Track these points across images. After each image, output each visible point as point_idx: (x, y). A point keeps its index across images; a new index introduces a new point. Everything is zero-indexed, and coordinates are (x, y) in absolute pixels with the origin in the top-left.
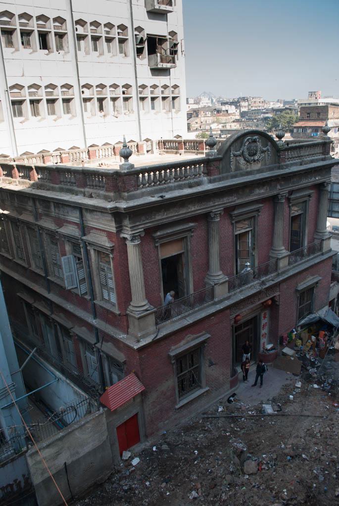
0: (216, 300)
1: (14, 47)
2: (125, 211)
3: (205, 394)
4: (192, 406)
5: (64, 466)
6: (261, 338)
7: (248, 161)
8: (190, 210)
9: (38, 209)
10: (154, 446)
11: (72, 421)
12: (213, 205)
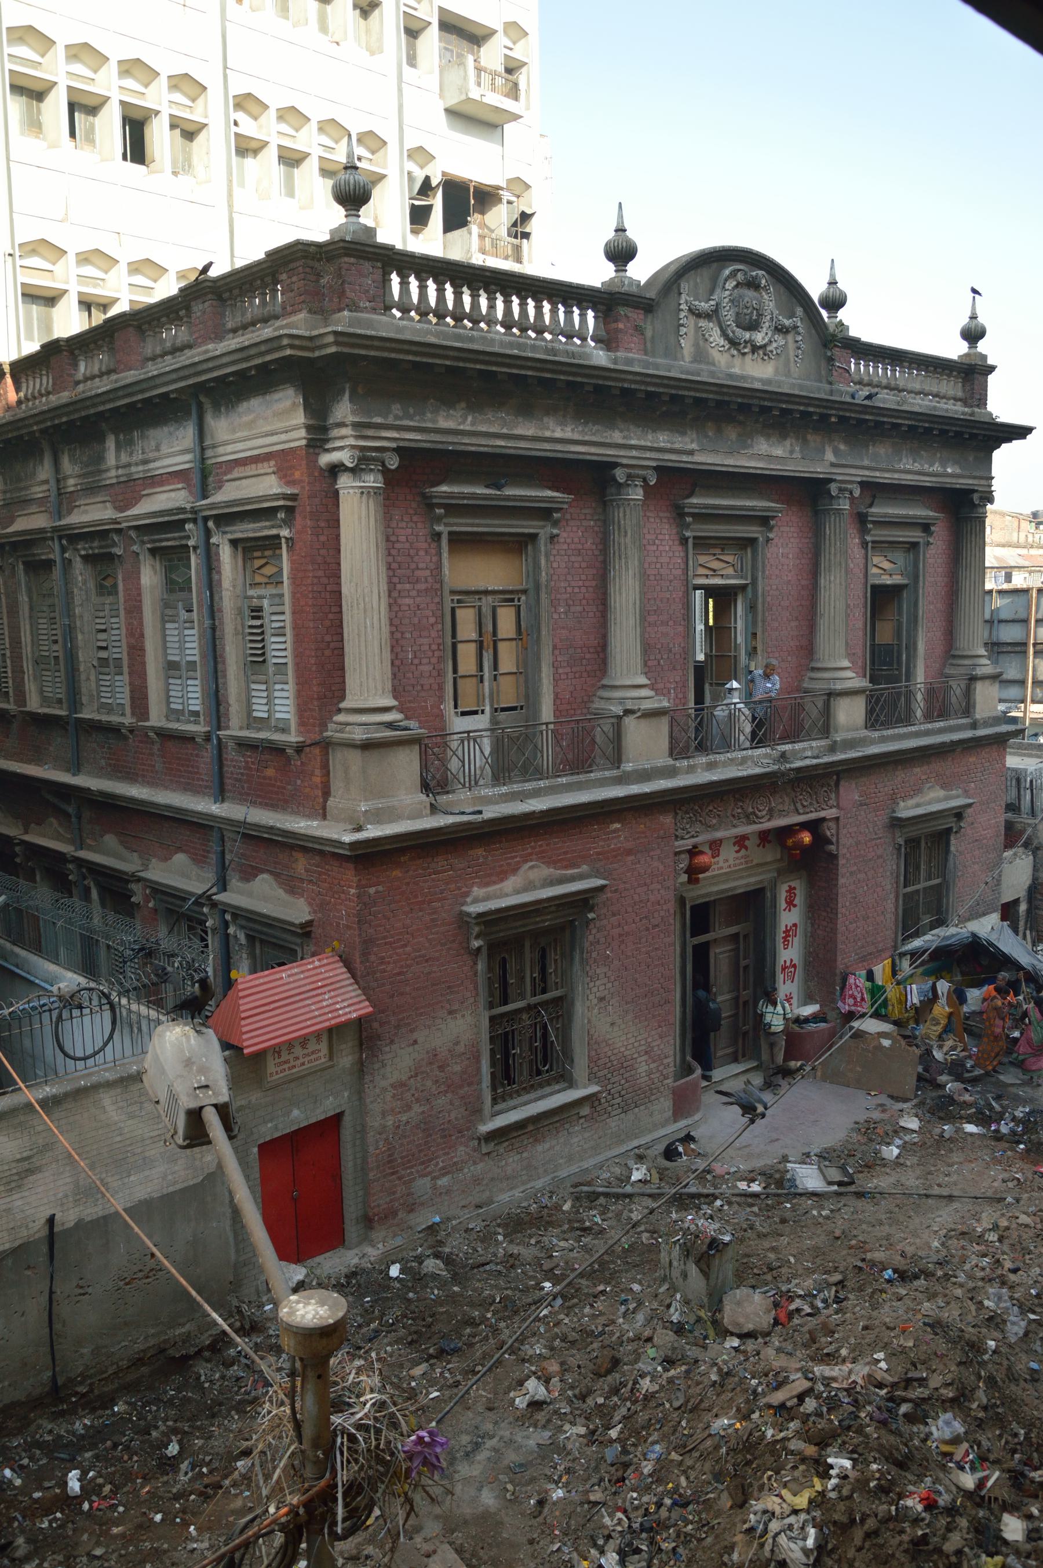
0: (628, 767)
1: (44, 139)
2: (350, 850)
3: (585, 1111)
4: (540, 1148)
5: (45, 1232)
6: (780, 977)
7: (734, 343)
8: (548, 434)
9: (65, 478)
10: (393, 1263)
11: (95, 1053)
12: (621, 441)
